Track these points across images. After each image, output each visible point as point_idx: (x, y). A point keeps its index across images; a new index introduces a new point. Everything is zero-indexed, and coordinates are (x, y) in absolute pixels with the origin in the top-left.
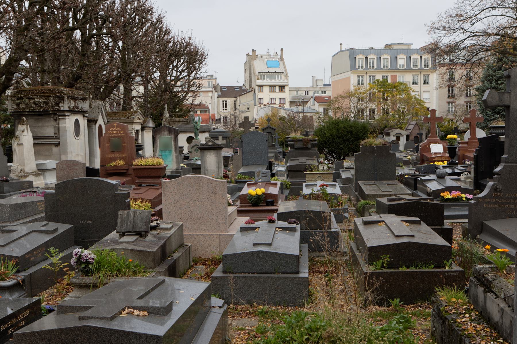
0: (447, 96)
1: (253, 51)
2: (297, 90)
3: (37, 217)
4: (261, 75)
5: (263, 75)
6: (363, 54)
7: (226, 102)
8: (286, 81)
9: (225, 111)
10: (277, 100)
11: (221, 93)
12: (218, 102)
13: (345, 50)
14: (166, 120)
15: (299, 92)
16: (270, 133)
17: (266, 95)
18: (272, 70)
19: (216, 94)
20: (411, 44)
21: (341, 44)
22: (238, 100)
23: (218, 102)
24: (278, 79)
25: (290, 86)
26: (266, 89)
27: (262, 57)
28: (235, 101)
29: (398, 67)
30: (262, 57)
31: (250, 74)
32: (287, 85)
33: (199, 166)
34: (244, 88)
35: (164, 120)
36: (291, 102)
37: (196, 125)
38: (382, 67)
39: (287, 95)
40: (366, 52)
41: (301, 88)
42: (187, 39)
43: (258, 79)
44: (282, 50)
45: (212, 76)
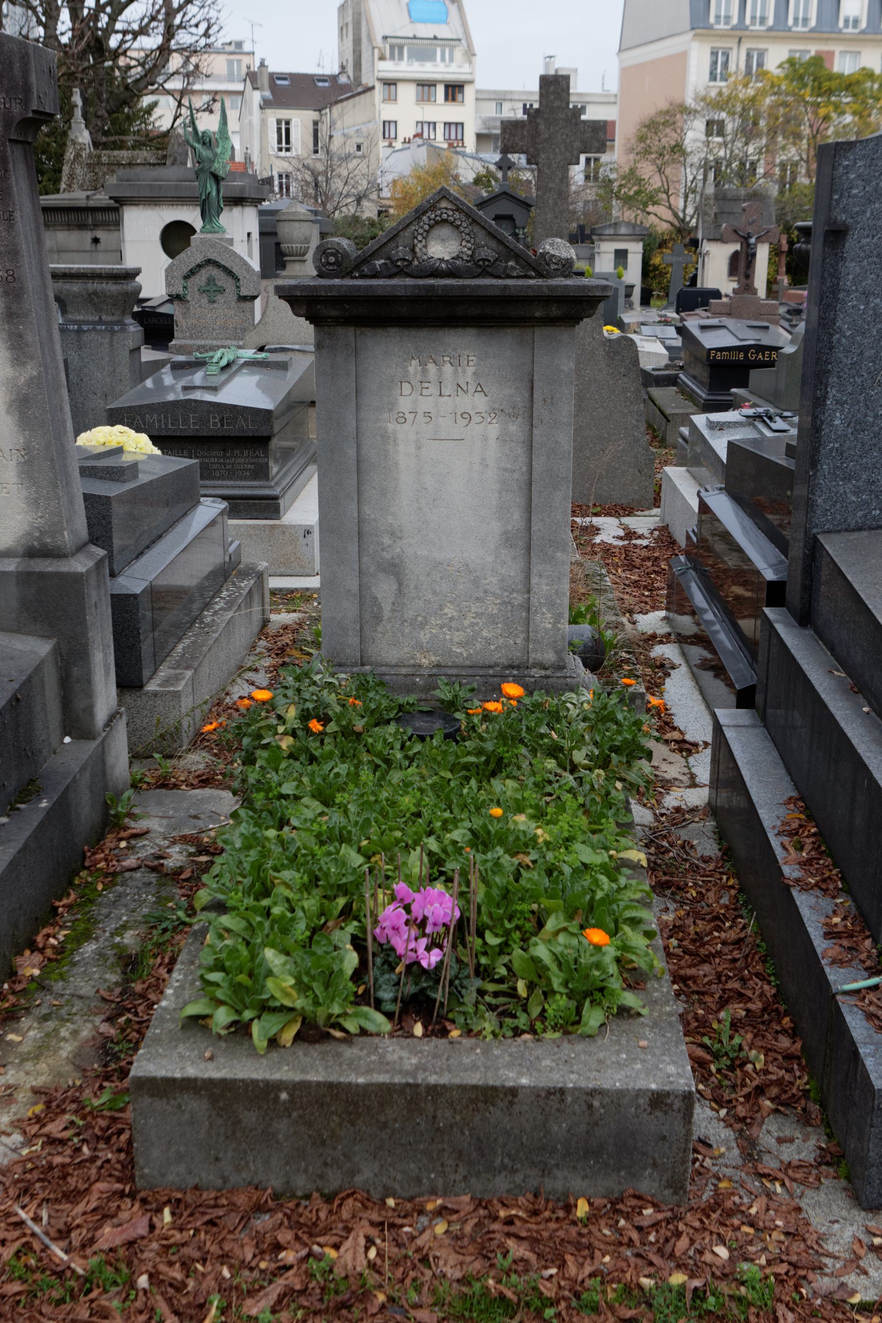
2: (500, 99)
4: (392, 47)
5: (396, 48)
7: (288, 123)
8: (466, 68)
9: (283, 154)
10: (440, 128)
11: (273, 93)
12: (263, 122)
14: (78, 156)
15: (506, 106)
16: (510, 218)
17: (406, 111)
18: (425, 31)
19: (256, 97)
22: (327, 119)
23: (263, 122)
24: (443, 59)
25: (480, 84)
26: (407, 93)
28: (316, 123)
29: (841, 24)
31: (357, 42)
32: (471, 82)
33: (250, 428)
34: (343, 80)
35: (70, 154)
36: (480, 137)
37: (205, 153)
38: (790, 22)
39: (469, 115)
41: (511, 92)
43: (382, 58)
45: (239, 44)
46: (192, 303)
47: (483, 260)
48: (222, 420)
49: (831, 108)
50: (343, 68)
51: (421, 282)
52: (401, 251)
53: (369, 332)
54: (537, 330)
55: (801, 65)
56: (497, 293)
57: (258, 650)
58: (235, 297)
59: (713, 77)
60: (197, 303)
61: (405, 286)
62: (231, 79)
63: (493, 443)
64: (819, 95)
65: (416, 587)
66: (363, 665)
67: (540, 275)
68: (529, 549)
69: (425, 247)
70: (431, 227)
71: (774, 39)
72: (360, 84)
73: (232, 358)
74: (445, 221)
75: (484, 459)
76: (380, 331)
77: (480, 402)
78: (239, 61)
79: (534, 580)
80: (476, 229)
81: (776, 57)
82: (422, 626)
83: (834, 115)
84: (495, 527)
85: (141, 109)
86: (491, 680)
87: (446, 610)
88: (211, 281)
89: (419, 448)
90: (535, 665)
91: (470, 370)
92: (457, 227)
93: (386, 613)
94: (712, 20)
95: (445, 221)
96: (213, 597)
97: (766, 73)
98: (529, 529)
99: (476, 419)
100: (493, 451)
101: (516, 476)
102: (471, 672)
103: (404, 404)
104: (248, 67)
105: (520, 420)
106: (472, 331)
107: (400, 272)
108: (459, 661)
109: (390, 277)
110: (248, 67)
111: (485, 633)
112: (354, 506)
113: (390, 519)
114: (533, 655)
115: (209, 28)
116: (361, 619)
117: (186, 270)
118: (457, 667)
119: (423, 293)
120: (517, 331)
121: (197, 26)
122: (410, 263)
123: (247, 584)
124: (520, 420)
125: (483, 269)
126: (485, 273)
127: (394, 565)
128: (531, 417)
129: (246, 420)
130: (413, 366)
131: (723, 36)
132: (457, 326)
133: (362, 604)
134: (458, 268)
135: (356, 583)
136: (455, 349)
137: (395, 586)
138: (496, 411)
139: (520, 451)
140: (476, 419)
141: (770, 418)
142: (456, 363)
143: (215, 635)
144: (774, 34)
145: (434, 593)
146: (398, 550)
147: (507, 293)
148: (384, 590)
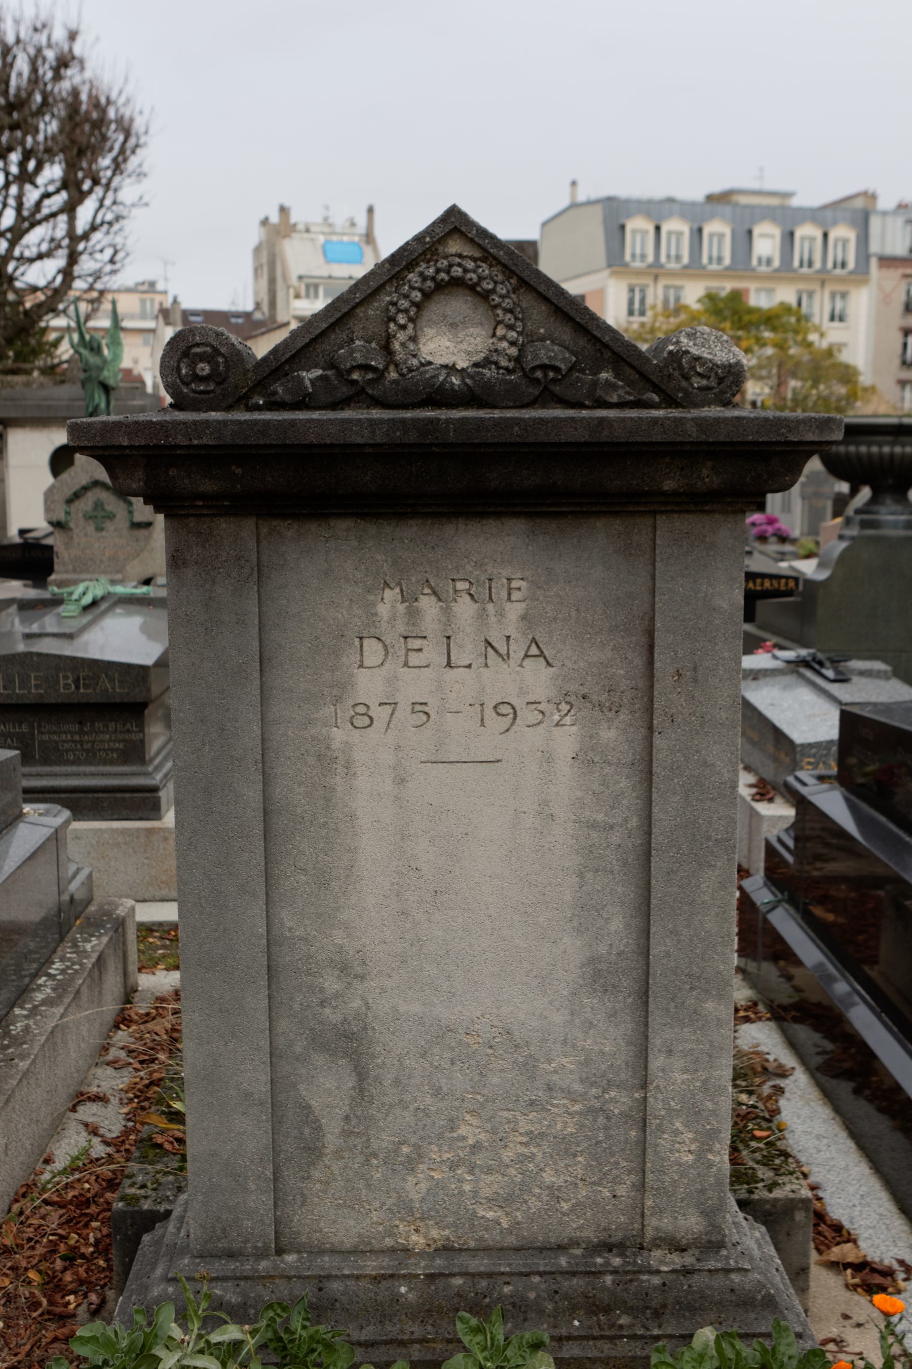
0: (897, 361)
1: (283, 210)
3: (376, 414)
4: (308, 287)
6: (648, 215)
13: (589, 203)
20: (788, 195)
21: (574, 184)
27: (308, 231)
29: (754, 262)
30: (308, 231)
31: (272, 282)
33: (117, 691)
34: (258, 316)
37: (93, 360)
40: (658, 210)
42: (59, 34)
43: (297, 296)
44: (370, 210)
45: (152, 284)
46: (76, 531)
47: (544, 367)
48: (77, 681)
49: (753, 341)
50: (258, 306)
51: (408, 414)
52: (359, 349)
53: (289, 530)
54: (661, 520)
55: (722, 300)
56: (583, 436)
57: (113, 1053)
58: (128, 524)
59: (631, 313)
60: (82, 531)
61: (372, 422)
62: (143, 316)
63: (564, 768)
64: (739, 328)
65: (397, 1082)
66: (280, 1252)
67: (670, 401)
68: (644, 994)
69: (414, 339)
70: (427, 296)
71: (691, 276)
72: (274, 321)
73: (99, 592)
74: (457, 283)
75: (545, 804)
76: (313, 527)
77: (538, 679)
78: (152, 300)
79: (657, 1062)
80: (527, 301)
81: (693, 294)
82: (410, 1165)
83: (756, 348)
84: (571, 950)
85: (47, 343)
86: (567, 1284)
87: (463, 1130)
88: (99, 505)
89: (401, 781)
90: (658, 1242)
91: (514, 611)
92: (485, 296)
93: (332, 1139)
94: (628, 257)
95: (457, 283)
96: (35, 975)
97: (686, 307)
98: (645, 951)
99: (528, 715)
100: (565, 783)
101: (615, 838)
102: (518, 1263)
103: (369, 685)
104: (161, 304)
105: (624, 716)
106: (519, 525)
107: (359, 396)
108: (491, 1238)
109: (335, 406)
110: (161, 304)
111: (548, 1177)
112: (257, 910)
113: (339, 936)
114: (653, 1222)
115: (116, 252)
116: (276, 1151)
117: (68, 492)
118: (487, 1250)
119: (413, 438)
120: (617, 524)
121: (101, 251)
122: (380, 374)
123: (94, 945)
124: (624, 716)
125: (544, 385)
126: (546, 397)
127: (349, 1036)
128: (650, 710)
129: (111, 680)
130: (388, 604)
131: (639, 273)
132: (482, 515)
133: (277, 1120)
134: (488, 386)
135: (264, 1077)
136: (479, 565)
137: (350, 1082)
138: (572, 699)
139: (624, 783)
140: (528, 715)
141: (821, 664)
142: (483, 595)
143: (23, 1065)
144: (689, 271)
145: (437, 1092)
146: (357, 1003)
147: (604, 436)
148: (326, 1089)
